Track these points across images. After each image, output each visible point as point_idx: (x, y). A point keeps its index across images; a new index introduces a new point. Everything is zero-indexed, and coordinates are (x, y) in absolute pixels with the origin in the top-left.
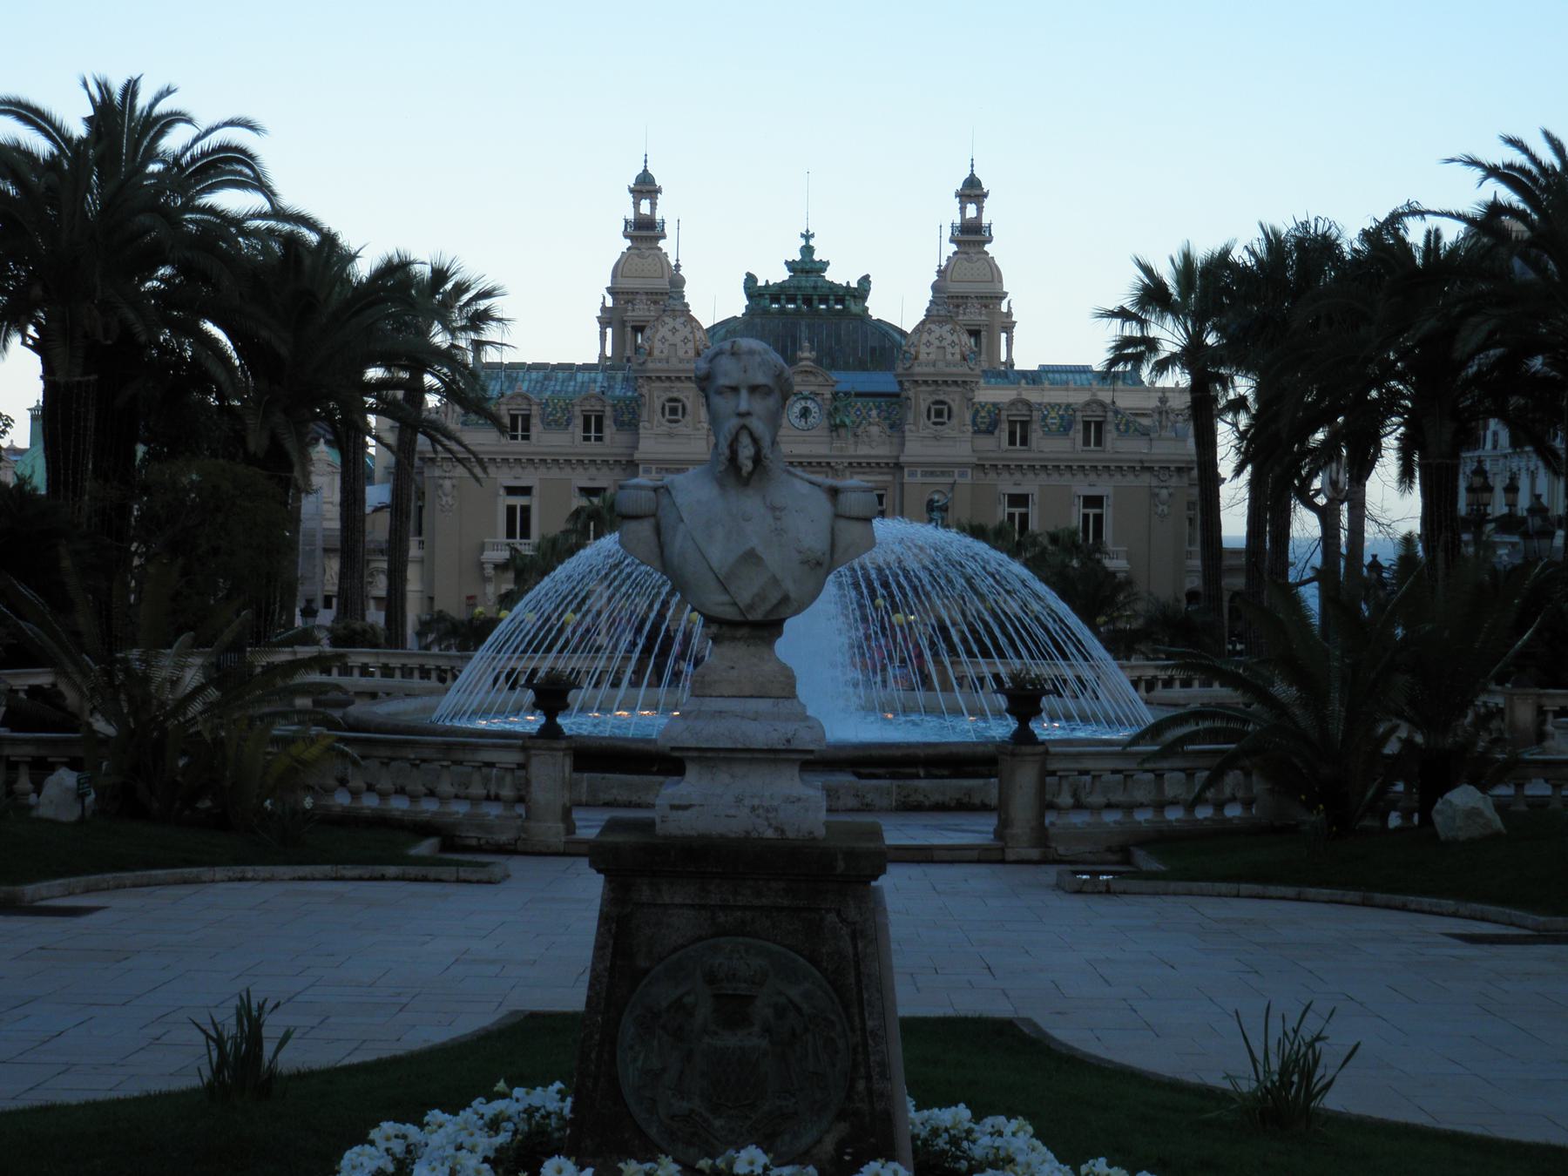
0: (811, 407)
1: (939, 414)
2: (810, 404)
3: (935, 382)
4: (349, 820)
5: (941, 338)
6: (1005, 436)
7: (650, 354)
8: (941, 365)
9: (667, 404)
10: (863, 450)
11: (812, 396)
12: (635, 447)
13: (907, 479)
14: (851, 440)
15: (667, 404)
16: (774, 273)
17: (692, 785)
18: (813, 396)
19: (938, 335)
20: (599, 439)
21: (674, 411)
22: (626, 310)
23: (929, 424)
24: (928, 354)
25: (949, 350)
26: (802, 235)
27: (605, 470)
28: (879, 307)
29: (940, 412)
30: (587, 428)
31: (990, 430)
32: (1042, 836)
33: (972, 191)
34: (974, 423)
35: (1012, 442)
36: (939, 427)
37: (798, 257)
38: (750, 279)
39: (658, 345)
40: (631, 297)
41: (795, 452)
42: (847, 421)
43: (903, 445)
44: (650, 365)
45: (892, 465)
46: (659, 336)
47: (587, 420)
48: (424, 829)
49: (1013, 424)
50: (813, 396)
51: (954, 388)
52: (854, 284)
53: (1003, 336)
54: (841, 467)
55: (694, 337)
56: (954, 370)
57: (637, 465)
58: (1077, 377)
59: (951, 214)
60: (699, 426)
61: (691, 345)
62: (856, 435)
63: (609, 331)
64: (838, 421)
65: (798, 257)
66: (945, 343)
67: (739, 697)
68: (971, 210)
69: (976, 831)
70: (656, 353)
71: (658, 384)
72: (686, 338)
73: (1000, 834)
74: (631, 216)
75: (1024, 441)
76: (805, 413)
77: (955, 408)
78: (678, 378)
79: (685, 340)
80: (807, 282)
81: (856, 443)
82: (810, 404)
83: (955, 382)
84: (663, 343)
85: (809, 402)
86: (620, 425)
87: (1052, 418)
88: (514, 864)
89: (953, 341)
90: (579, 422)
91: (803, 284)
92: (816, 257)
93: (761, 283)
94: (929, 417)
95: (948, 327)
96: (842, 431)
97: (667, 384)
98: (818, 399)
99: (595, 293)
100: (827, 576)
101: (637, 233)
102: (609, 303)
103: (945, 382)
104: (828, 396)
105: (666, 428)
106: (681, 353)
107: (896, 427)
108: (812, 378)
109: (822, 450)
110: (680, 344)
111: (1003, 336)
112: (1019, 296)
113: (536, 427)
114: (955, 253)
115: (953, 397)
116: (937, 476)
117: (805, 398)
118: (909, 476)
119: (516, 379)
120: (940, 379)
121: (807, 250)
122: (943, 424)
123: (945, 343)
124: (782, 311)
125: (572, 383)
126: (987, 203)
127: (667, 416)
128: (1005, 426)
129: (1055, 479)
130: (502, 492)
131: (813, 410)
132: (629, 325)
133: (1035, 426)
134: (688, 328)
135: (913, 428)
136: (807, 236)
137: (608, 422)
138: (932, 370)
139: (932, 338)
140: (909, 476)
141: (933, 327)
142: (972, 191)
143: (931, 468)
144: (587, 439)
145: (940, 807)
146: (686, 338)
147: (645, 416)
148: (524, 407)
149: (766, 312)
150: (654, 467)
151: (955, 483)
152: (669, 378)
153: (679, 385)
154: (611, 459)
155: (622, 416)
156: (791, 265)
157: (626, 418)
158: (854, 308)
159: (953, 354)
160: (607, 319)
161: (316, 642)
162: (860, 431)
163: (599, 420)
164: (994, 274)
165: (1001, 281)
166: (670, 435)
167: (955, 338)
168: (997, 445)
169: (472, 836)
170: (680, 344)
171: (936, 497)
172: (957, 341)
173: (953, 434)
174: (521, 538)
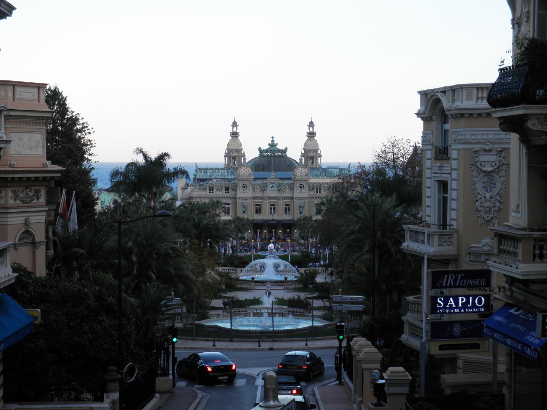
1: (301, 187)
2: (274, 185)
3: (300, 180)
4: (241, 288)
5: (301, 171)
6: (316, 191)
7: (239, 175)
8: (301, 177)
10: (285, 195)
12: (236, 194)
13: (294, 201)
14: (282, 192)
16: (265, 147)
17: (334, 380)
18: (274, 183)
20: (228, 193)
21: (244, 187)
22: (231, 154)
23: (299, 189)
25: (303, 173)
27: (230, 199)
28: (289, 154)
29: (301, 187)
30: (226, 190)
31: (312, 190)
32: (287, 288)
33: (311, 124)
34: (309, 188)
35: (317, 192)
36: (301, 190)
38: (260, 149)
39: (241, 173)
40: (232, 151)
41: (270, 195)
42: (282, 189)
43: (294, 193)
44: (239, 177)
46: (241, 171)
47: (226, 188)
48: (244, 288)
49: (317, 188)
50: (274, 183)
52: (283, 150)
53: (319, 158)
56: (304, 178)
58: (335, 170)
59: (307, 130)
61: (248, 173)
62: (283, 192)
63: (227, 158)
65: (271, 143)
66: (302, 172)
68: (311, 129)
69: (282, 287)
70: (240, 174)
71: (241, 181)
73: (284, 288)
75: (320, 192)
76: (273, 187)
77: (305, 186)
78: (245, 180)
79: (247, 172)
80: (273, 149)
81: (284, 193)
82: (274, 185)
83: (305, 180)
86: (233, 189)
88: (252, 291)
90: (224, 189)
91: (272, 149)
92: (275, 142)
93: (262, 149)
95: (303, 168)
96: (281, 191)
97: (243, 181)
98: (275, 184)
99: (223, 149)
101: (233, 136)
103: (302, 180)
104: (277, 183)
106: (246, 174)
107: (292, 189)
108: (274, 180)
109: (276, 195)
110: (246, 173)
111: (319, 158)
112: (323, 148)
113: (215, 190)
114: (307, 139)
115: (304, 184)
117: (273, 184)
119: (206, 172)
120: (301, 180)
121: (273, 141)
123: (302, 172)
124: (267, 155)
125: (219, 173)
126: (315, 127)
128: (316, 189)
132: (232, 157)
133: (322, 189)
136: (273, 138)
137: (230, 189)
139: (300, 171)
141: (300, 168)
142: (311, 124)
143: (299, 199)
144: (226, 193)
145: (281, 286)
147: (238, 188)
149: (264, 156)
151: (304, 202)
152: (243, 180)
153: (245, 181)
154: (231, 197)
156: (269, 144)
157: (234, 188)
158: (284, 155)
160: (226, 155)
162: (284, 190)
163: (228, 189)
164: (317, 145)
165: (318, 146)
166: (244, 192)
167: (304, 170)
168: (314, 193)
169: (247, 289)
170: (246, 173)
171: (301, 205)
173: (305, 191)
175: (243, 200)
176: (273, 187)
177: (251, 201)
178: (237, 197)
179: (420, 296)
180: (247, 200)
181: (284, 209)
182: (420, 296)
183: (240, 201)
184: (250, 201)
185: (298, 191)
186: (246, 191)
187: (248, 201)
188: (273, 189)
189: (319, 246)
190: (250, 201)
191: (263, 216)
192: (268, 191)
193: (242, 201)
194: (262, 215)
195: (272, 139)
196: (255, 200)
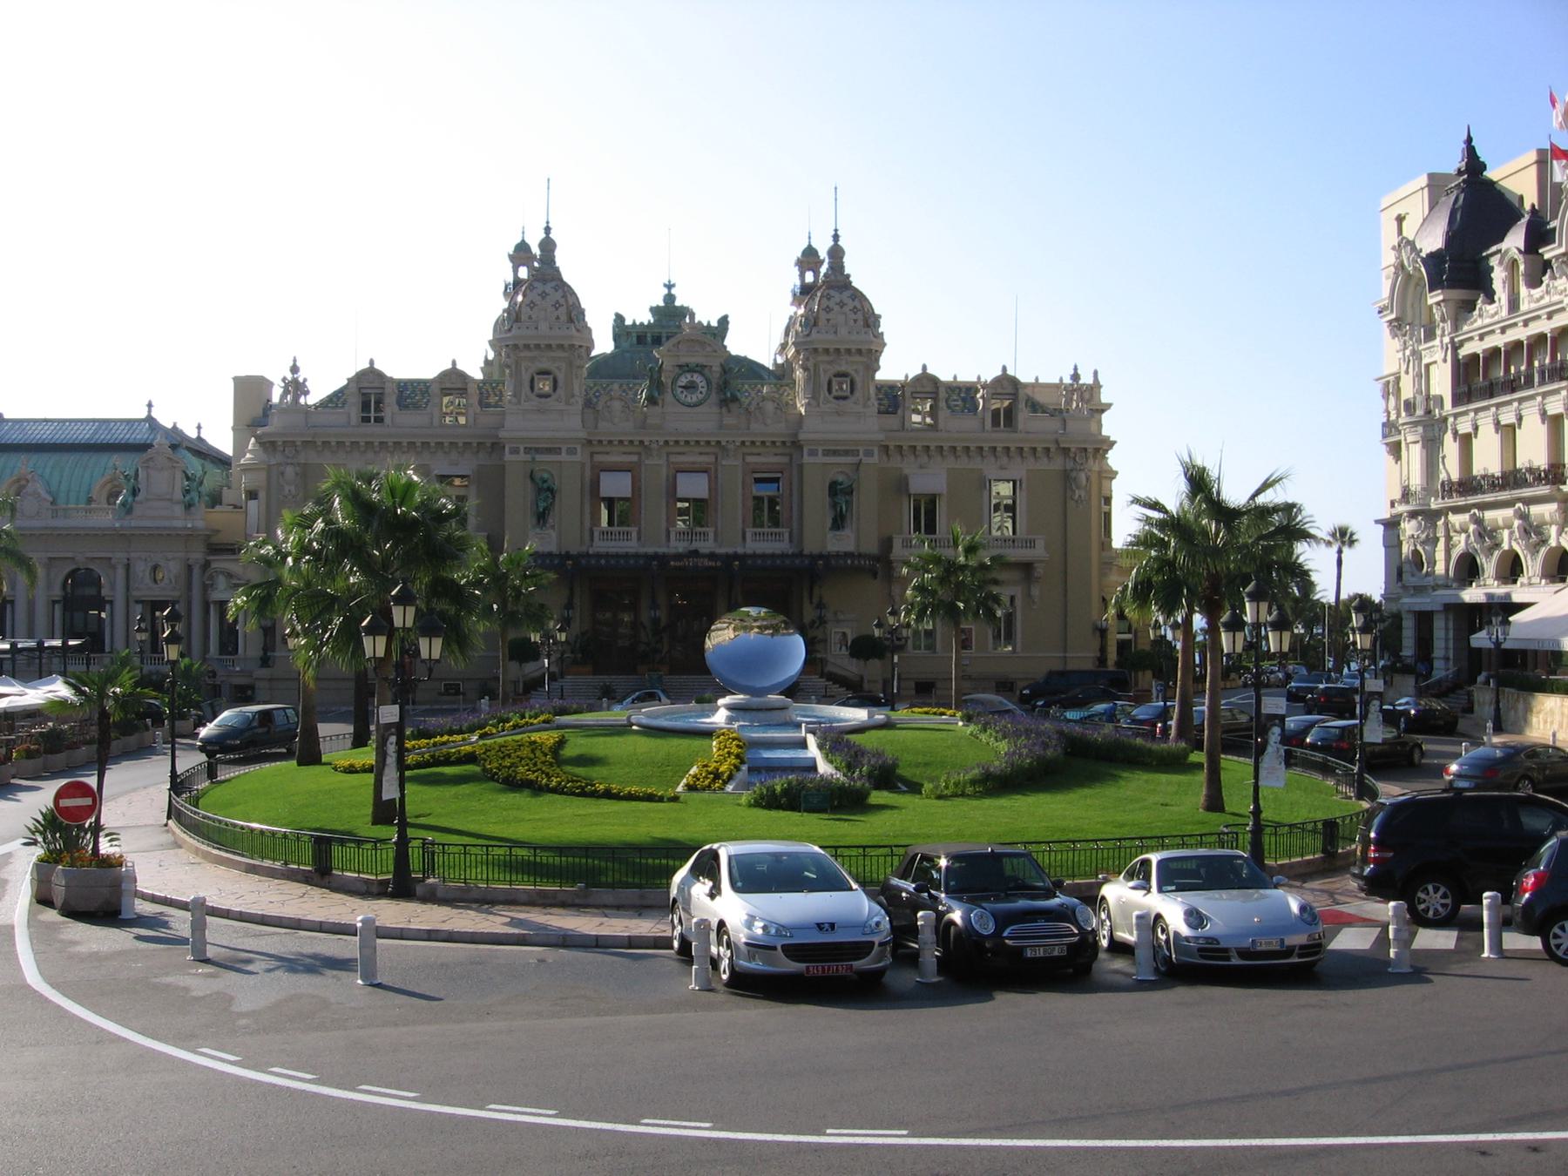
0: (698, 381)
2: (697, 378)
19: (838, 301)
20: (379, 420)
26: (665, 285)
37: (662, 304)
38: (619, 319)
51: (858, 358)
52: (714, 324)
55: (567, 301)
60: (572, 400)
65: (662, 304)
67: (128, 618)
72: (557, 302)
74: (510, 279)
85: (695, 376)
87: (955, 400)
89: (855, 307)
92: (678, 303)
93: (628, 322)
94: (830, 390)
96: (733, 407)
97: (535, 353)
100: (203, 998)
102: (491, 356)
116: (840, 455)
117: (692, 371)
121: (670, 298)
123: (846, 309)
129: (963, 463)
131: (700, 385)
134: (560, 292)
136: (669, 286)
140: (511, 453)
146: (557, 302)
151: (859, 464)
155: (487, 398)
159: (855, 321)
172: (859, 307)
176: (691, 387)
177: (578, 458)
178: (802, 436)
179: (766, 501)
180: (557, 451)
182: (766, 501)
183: (522, 457)
187: (564, 457)
188: (693, 398)
191: (639, 539)
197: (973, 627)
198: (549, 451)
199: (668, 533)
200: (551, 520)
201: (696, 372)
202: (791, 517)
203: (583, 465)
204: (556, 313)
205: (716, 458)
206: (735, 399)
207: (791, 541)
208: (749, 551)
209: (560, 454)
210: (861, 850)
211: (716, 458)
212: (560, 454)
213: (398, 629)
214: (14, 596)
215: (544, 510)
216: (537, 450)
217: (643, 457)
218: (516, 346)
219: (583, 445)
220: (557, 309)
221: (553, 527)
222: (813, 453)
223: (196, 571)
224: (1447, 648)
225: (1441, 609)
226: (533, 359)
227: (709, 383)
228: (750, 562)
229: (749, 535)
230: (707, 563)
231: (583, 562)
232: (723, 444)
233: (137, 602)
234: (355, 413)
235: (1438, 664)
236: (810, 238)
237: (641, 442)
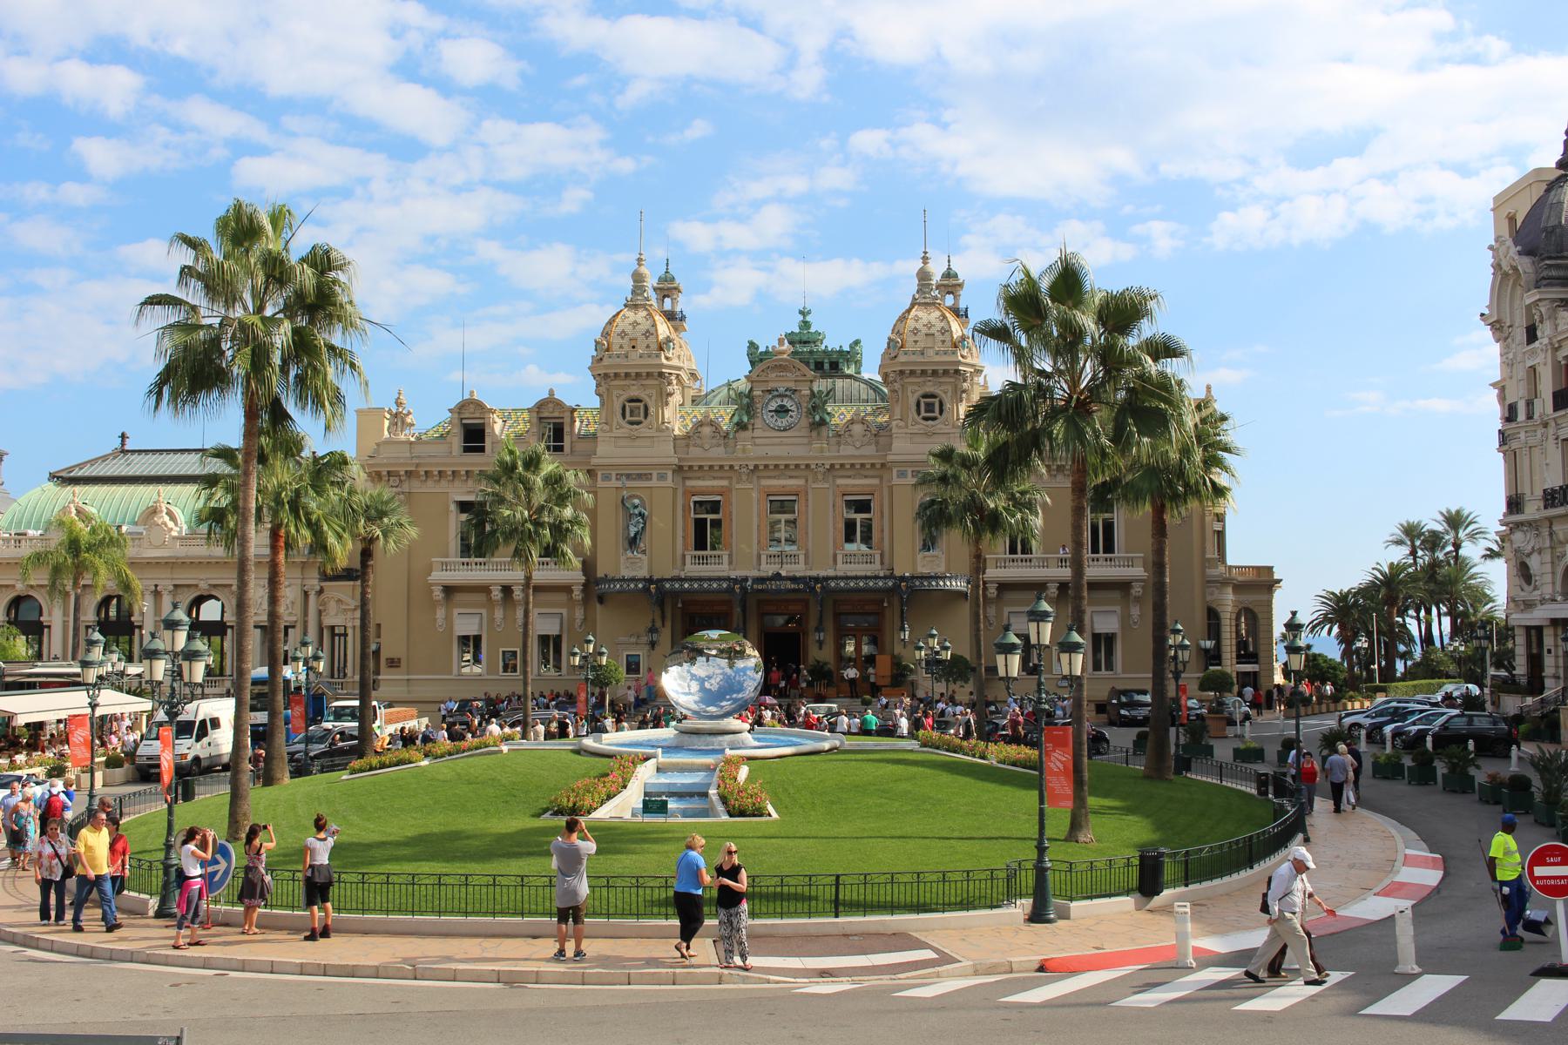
9: (922, 400)
11: (788, 393)
13: (896, 481)
15: (922, 400)
24: (916, 342)
36: (930, 423)
38: (752, 345)
45: (878, 466)
54: (821, 469)
57: (890, 469)
64: (817, 418)
70: (615, 347)
81: (839, 444)
82: (787, 403)
84: (622, 338)
85: (786, 400)
93: (762, 349)
105: (627, 429)
109: (800, 451)
110: (641, 338)
116: (634, 479)
117: (781, 396)
118: (603, 480)
121: (805, 325)
122: (934, 419)
127: (923, 414)
130: (453, 507)
135: (902, 424)
138: (920, 359)
140: (603, 480)
148: (477, 415)
150: (614, 473)
161: (1366, 688)
174: (1104, 553)
175: (628, 476)
176: (782, 411)
180: (648, 477)
181: (841, 526)
184: (662, 484)
185: (915, 429)
186: (642, 430)
187: (654, 483)
188: (783, 422)
189: (1455, 631)
190: (662, 484)
191: (730, 563)
192: (757, 433)
193: (619, 484)
194: (726, 559)
195: (801, 318)
196: (689, 483)
197: (625, 654)
198: (640, 477)
199: (835, 556)
200: (642, 545)
201: (786, 396)
202: (883, 539)
203: (675, 490)
204: (647, 342)
205: (807, 481)
206: (823, 422)
207: (882, 563)
208: (840, 574)
209: (651, 479)
210: (384, 877)
211: (807, 481)
212: (651, 479)
213: (1034, 646)
214: (50, 621)
215: (636, 535)
216: (628, 476)
217: (810, 481)
218: (606, 376)
219: (674, 471)
220: (647, 338)
221: (644, 552)
222: (607, 478)
223: (312, 598)
224: (1557, 667)
225: (1548, 623)
226: (624, 388)
227: (799, 406)
228: (833, 584)
229: (688, 559)
230: (790, 585)
231: (668, 586)
232: (737, 468)
233: (255, 627)
234: (457, 442)
235: (1548, 682)
236: (949, 261)
237: (731, 467)
